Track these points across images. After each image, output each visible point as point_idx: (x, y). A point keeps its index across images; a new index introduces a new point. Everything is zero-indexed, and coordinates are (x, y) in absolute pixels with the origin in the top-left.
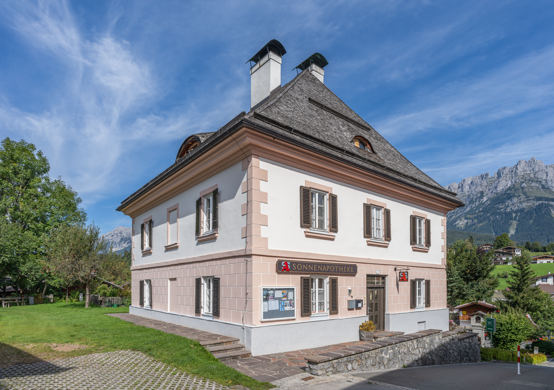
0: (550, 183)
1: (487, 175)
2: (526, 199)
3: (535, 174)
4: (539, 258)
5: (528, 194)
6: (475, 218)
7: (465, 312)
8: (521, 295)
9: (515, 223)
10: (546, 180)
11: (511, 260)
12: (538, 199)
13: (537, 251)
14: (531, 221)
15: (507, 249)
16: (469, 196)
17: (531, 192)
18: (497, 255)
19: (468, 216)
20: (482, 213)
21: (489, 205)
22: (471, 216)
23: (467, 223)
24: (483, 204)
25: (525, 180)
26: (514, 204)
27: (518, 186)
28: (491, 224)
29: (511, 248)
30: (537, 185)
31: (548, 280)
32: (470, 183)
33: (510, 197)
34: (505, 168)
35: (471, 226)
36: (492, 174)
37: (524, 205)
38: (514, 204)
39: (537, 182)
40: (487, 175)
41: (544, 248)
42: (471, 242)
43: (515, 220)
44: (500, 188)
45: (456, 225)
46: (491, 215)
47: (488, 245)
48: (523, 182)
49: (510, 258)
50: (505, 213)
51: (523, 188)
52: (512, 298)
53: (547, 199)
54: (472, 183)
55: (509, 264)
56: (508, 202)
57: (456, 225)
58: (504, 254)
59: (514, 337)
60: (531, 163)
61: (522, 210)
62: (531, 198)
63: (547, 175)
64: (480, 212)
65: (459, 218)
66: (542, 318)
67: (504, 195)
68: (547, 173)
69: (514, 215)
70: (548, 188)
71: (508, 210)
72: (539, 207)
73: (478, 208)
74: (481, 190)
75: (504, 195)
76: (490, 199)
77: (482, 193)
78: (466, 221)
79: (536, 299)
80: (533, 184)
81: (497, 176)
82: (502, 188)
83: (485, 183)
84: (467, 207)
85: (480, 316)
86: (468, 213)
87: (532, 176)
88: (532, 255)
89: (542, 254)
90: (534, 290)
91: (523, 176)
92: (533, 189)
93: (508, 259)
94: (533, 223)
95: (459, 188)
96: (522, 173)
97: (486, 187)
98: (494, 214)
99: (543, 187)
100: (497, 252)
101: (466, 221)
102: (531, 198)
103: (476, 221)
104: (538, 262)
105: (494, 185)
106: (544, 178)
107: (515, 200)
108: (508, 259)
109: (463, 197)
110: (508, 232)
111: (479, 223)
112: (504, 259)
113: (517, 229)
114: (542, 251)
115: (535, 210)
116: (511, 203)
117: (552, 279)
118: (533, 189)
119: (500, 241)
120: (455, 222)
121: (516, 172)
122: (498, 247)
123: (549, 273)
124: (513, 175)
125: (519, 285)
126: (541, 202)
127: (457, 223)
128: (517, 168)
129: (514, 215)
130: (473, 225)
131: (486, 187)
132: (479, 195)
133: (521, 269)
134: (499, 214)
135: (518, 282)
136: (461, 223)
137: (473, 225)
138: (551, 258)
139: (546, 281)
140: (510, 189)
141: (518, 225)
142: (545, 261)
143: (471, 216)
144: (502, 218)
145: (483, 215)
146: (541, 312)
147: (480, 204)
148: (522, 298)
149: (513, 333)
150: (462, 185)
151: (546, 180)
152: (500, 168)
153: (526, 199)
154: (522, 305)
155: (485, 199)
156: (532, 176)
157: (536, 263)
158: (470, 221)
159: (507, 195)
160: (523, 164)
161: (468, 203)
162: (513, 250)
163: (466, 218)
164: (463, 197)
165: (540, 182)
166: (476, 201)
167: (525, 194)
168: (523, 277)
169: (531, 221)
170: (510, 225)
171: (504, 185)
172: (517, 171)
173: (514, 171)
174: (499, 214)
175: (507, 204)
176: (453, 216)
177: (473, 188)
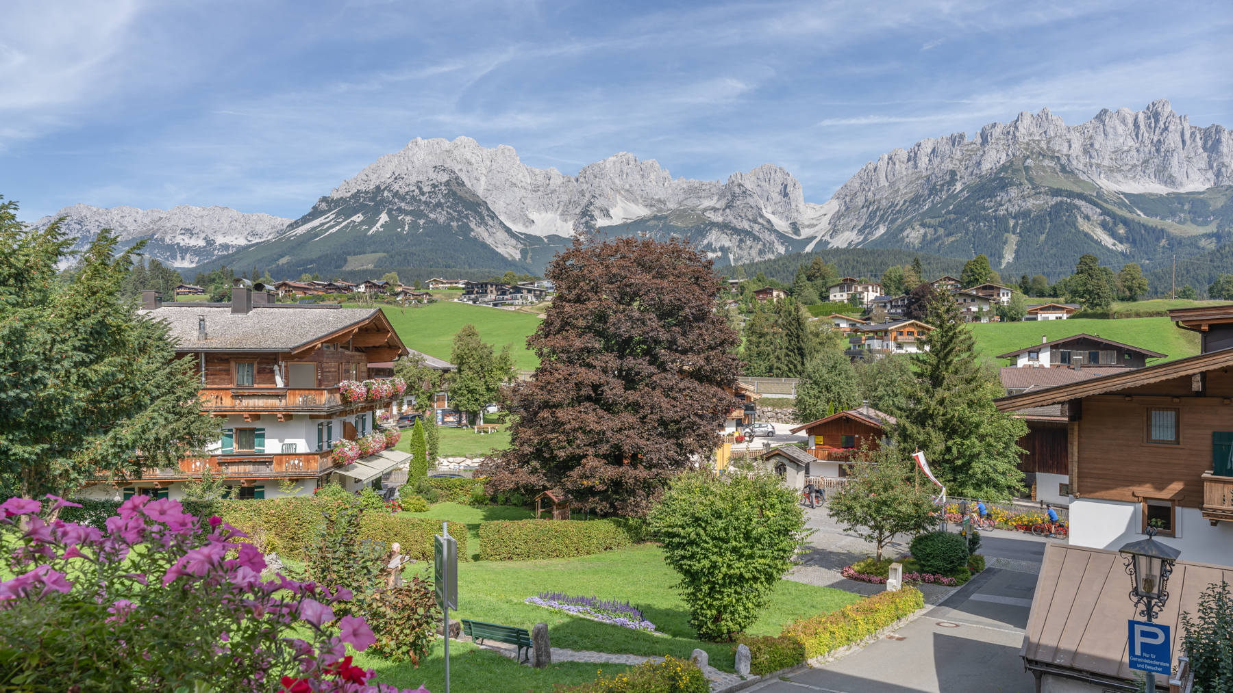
0: (1075, 162)
1: (962, 136)
2: (1033, 192)
3: (1048, 143)
4: (1042, 309)
5: (1037, 182)
6: (940, 225)
7: (821, 439)
8: (940, 393)
9: (1013, 239)
10: (1068, 156)
11: (989, 312)
12: (1056, 192)
13: (1041, 294)
14: (1042, 237)
15: (985, 288)
16: (928, 178)
17: (1042, 178)
18: (961, 301)
19: (928, 220)
20: (952, 216)
21: (966, 199)
22: (932, 221)
23: (925, 235)
24: (955, 197)
25: (1032, 153)
26: (1013, 201)
27: (1018, 164)
28: (969, 240)
29: (991, 288)
30: (1053, 164)
31: (1041, 355)
32: (929, 150)
33: (1004, 185)
34: (994, 125)
35: (931, 242)
36: (972, 136)
37: (1030, 203)
38: (1013, 201)
39: (1052, 158)
40: (962, 136)
41: (1055, 289)
42: (917, 272)
43: (1014, 233)
44: (986, 166)
45: (903, 239)
46: (970, 220)
47: (950, 279)
48: (1028, 157)
49: (986, 308)
50: (995, 218)
51: (1027, 169)
52: (919, 401)
53: (1070, 194)
54: (933, 151)
55: (984, 321)
56: (1002, 196)
57: (903, 239)
58: (974, 298)
59: (739, 567)
60: (1042, 118)
61: (1025, 214)
62: (1043, 190)
63: (1070, 146)
64: (949, 212)
65: (909, 223)
66: (984, 455)
67: (994, 180)
68: (1069, 141)
69: (1012, 222)
70: (1072, 172)
71: (1002, 212)
72: (1056, 210)
73: (945, 203)
74: (951, 167)
75: (994, 180)
76: (968, 186)
77: (953, 173)
78: (922, 231)
79: (971, 404)
80: (1046, 163)
81: (980, 140)
82: (989, 166)
83: (959, 153)
84: (924, 201)
85: (786, 462)
86: (927, 214)
87: (1043, 145)
88: (1034, 302)
89: (1048, 301)
90: (968, 382)
91: (1028, 144)
92: (1045, 172)
93: (980, 309)
94: (1046, 242)
95: (909, 160)
96: (1027, 139)
97: (961, 161)
98: (976, 219)
99: (1063, 169)
100: (961, 294)
101: (922, 231)
102: (1043, 190)
103: (941, 231)
104: (1039, 318)
105: (975, 159)
106: (1065, 151)
107: (1014, 192)
108: (980, 309)
109: (918, 179)
110: (1001, 257)
111: (947, 236)
112: (974, 309)
113: (1016, 252)
114: (1050, 296)
115: (1050, 214)
116: (1006, 198)
117: (1048, 354)
118: (1045, 172)
119: (972, 271)
120: (902, 231)
121: (1014, 136)
122: (970, 284)
123: (1045, 340)
124: (1011, 142)
125: (936, 367)
126: (1059, 199)
127: (905, 233)
128: (1016, 128)
129: (1012, 222)
130: (937, 239)
131: (961, 161)
132: (948, 178)
133: (941, 326)
134: (985, 219)
135: (934, 360)
136: (913, 234)
137: (937, 239)
138: (1063, 309)
139: (1038, 359)
140: (1004, 168)
141: (1019, 244)
142: (1052, 316)
143: (932, 221)
144: (990, 227)
145: (955, 220)
146: (982, 438)
147: (949, 197)
148: (941, 402)
149: (735, 550)
150: (916, 154)
151: (1068, 156)
152: (986, 124)
153: (1033, 192)
154: (939, 423)
155: (959, 186)
156: (1043, 145)
157: (1035, 319)
158: (931, 231)
159: (999, 182)
160: (1026, 121)
161: (926, 192)
162: (995, 292)
163: (923, 225)
164: (918, 179)
165: (1058, 158)
166: (941, 191)
167: (1031, 180)
168: (945, 345)
169: (1042, 237)
170: (1005, 243)
171: (993, 159)
172: (1018, 134)
173: (1011, 132)
174: (985, 219)
175: (999, 198)
176: (897, 219)
177: (936, 161)
